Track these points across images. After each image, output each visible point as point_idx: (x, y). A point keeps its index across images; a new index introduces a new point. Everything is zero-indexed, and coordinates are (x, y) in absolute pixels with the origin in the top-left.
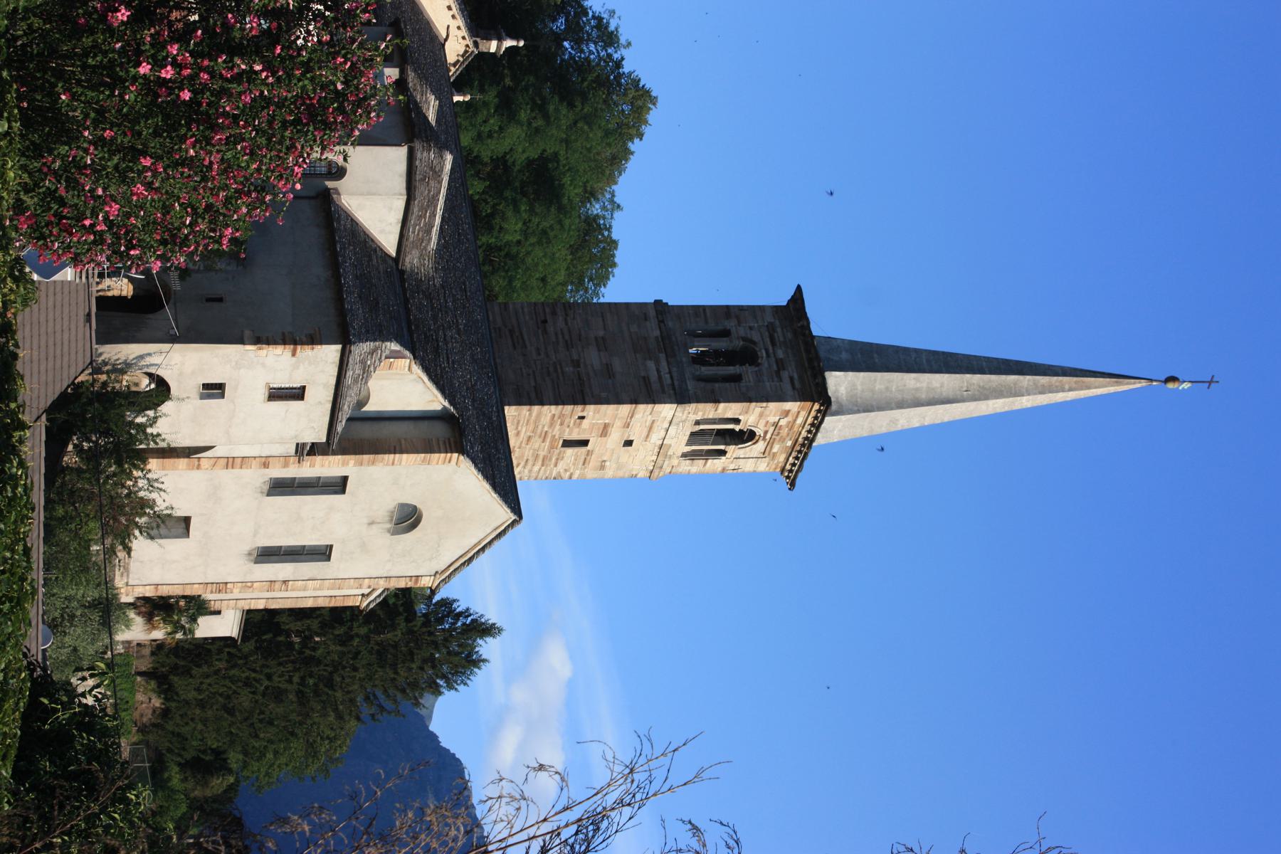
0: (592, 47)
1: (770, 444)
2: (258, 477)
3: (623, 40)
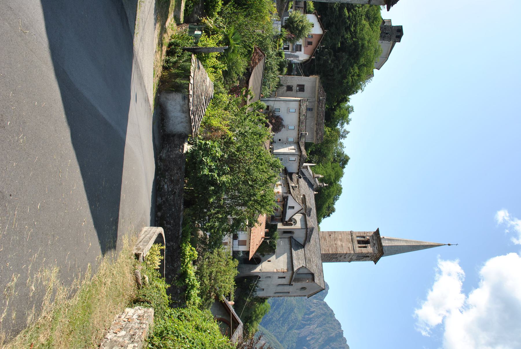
3: (344, 147)
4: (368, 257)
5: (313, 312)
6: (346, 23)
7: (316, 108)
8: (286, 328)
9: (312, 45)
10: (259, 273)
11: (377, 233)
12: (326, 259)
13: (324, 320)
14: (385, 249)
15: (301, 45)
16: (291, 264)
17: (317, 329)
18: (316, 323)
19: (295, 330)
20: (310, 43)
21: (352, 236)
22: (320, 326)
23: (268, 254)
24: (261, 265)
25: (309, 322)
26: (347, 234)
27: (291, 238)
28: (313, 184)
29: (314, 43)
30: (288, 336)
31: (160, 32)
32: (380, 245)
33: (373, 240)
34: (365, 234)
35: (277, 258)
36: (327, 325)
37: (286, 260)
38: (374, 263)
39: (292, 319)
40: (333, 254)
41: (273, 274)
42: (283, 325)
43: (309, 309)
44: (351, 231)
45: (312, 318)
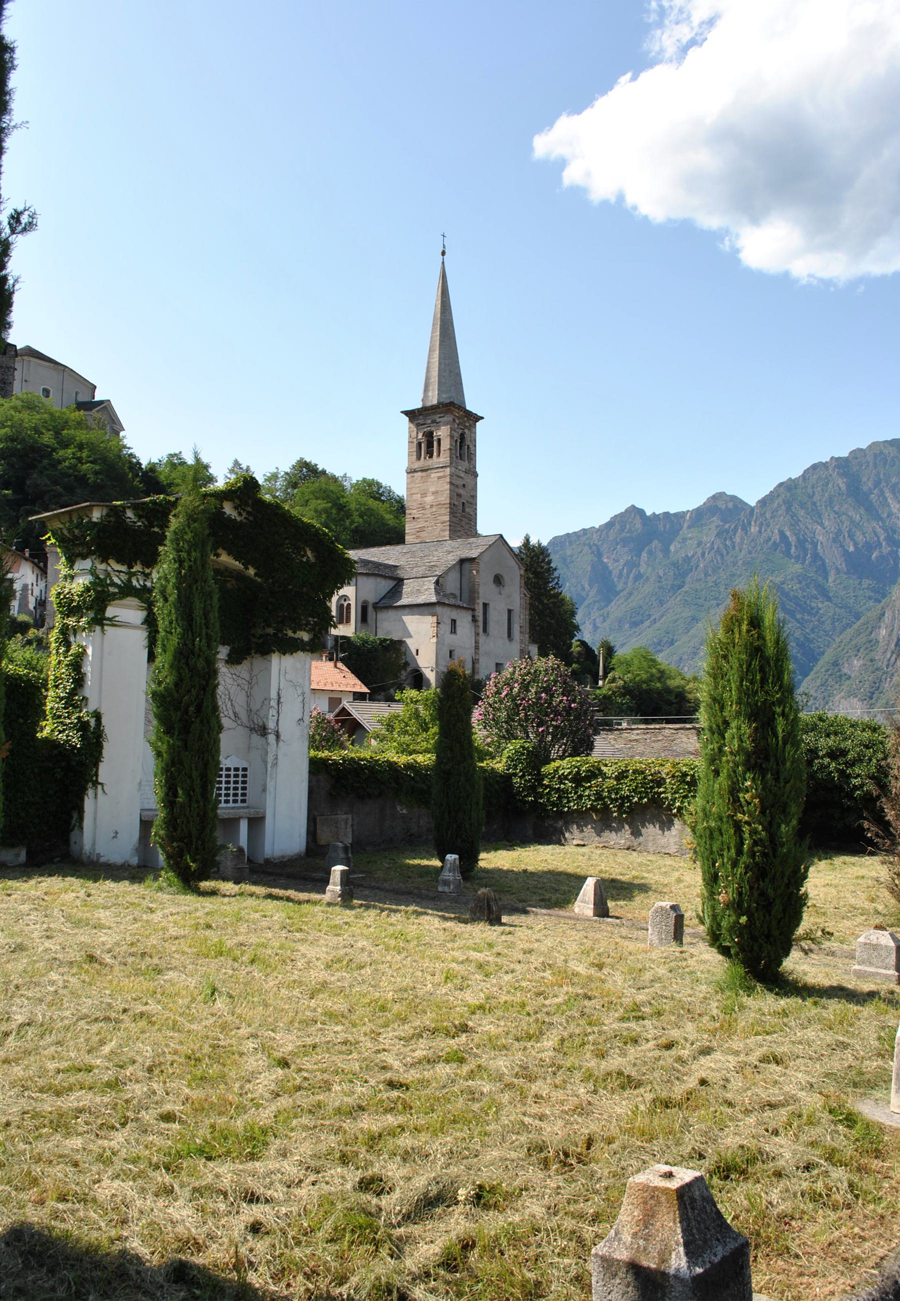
1: (466, 427)
2: (482, 638)
3: (275, 471)
4: (462, 436)
5: (782, 534)
8: (822, 605)
10: (437, 673)
11: (411, 415)
12: (467, 527)
13: (802, 505)
14: (446, 399)
16: (423, 608)
17: (826, 523)
18: (810, 527)
19: (827, 581)
21: (415, 471)
22: (820, 517)
23: (405, 654)
25: (808, 546)
26: (412, 482)
27: (377, 607)
30: (842, 599)
34: (412, 442)
35: (411, 636)
36: (816, 498)
37: (416, 618)
39: (801, 589)
40: (452, 513)
41: (444, 644)
42: (814, 611)
43: (775, 546)
44: (408, 473)
45: (798, 539)
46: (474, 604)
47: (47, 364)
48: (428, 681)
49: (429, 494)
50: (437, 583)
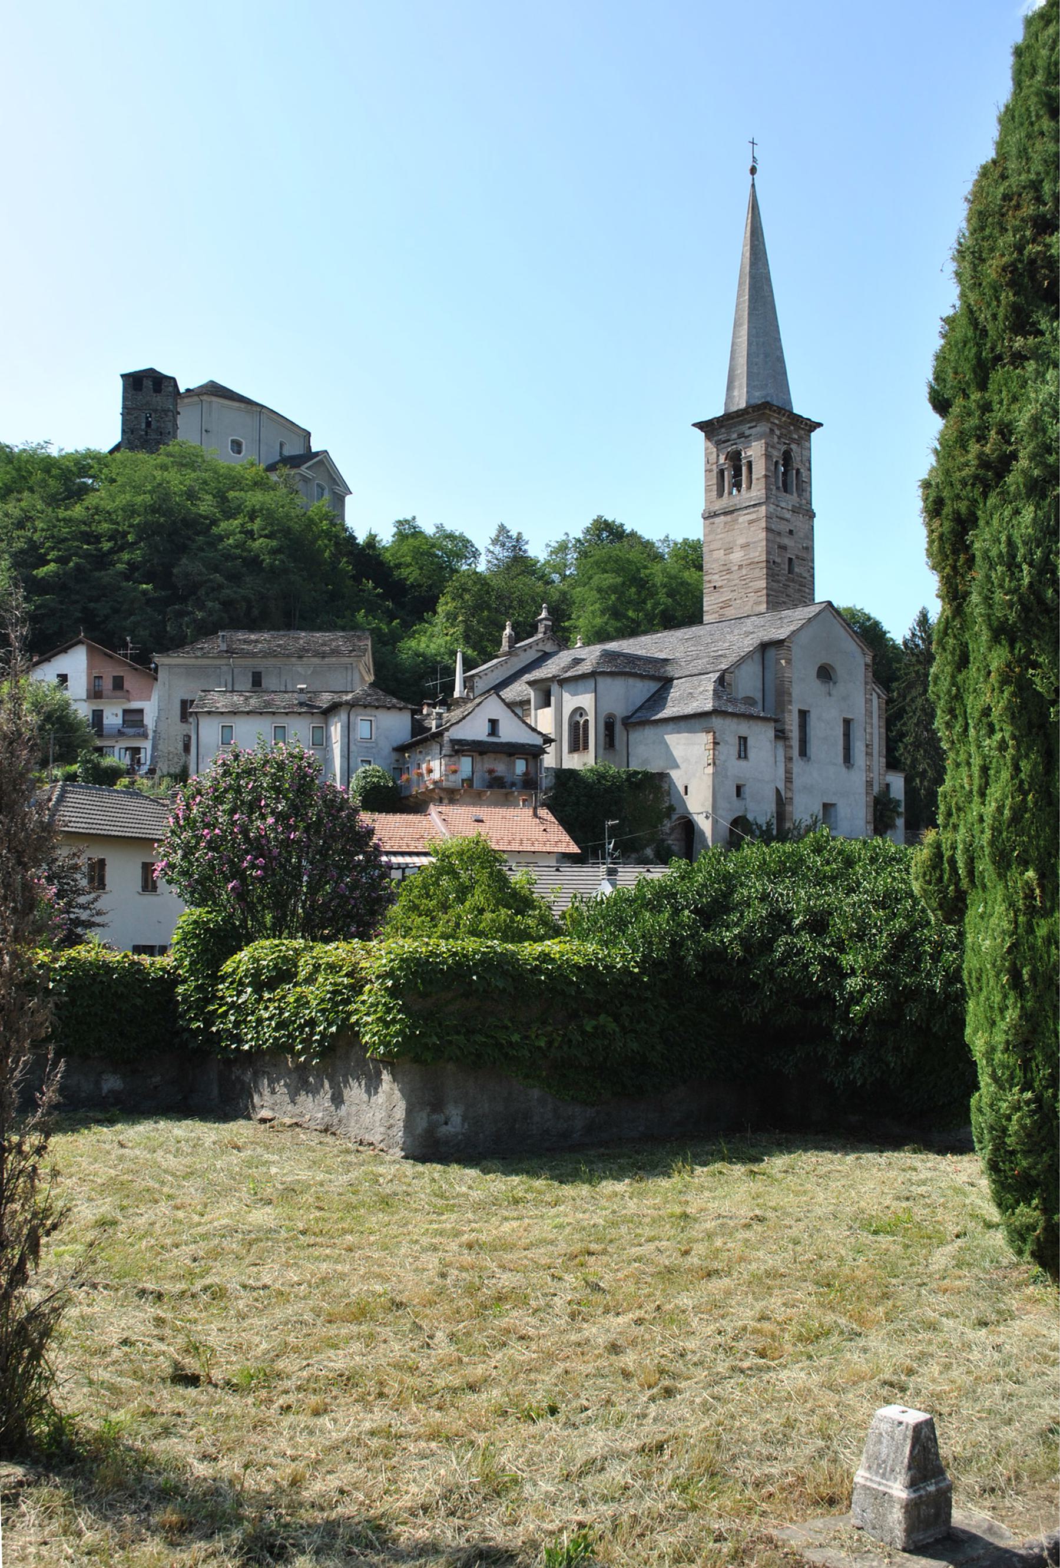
0: (569, 557)
1: (793, 440)
2: (798, 766)
3: (564, 538)
4: (787, 457)
6: (78, 567)
7: (249, 662)
9: (122, 677)
11: (708, 427)
14: (758, 398)
15: (125, 712)
16: (693, 721)
20: (118, 684)
21: (716, 515)
23: (669, 794)
24: (695, 817)
28: (540, 654)
29: (119, 671)
31: (517, 1175)
32: (743, 415)
33: (729, 440)
34: (710, 471)
35: (677, 766)
38: (818, 430)
41: (726, 777)
46: (783, 712)
47: (236, 404)
48: (703, 833)
49: (737, 549)
50: (721, 681)
